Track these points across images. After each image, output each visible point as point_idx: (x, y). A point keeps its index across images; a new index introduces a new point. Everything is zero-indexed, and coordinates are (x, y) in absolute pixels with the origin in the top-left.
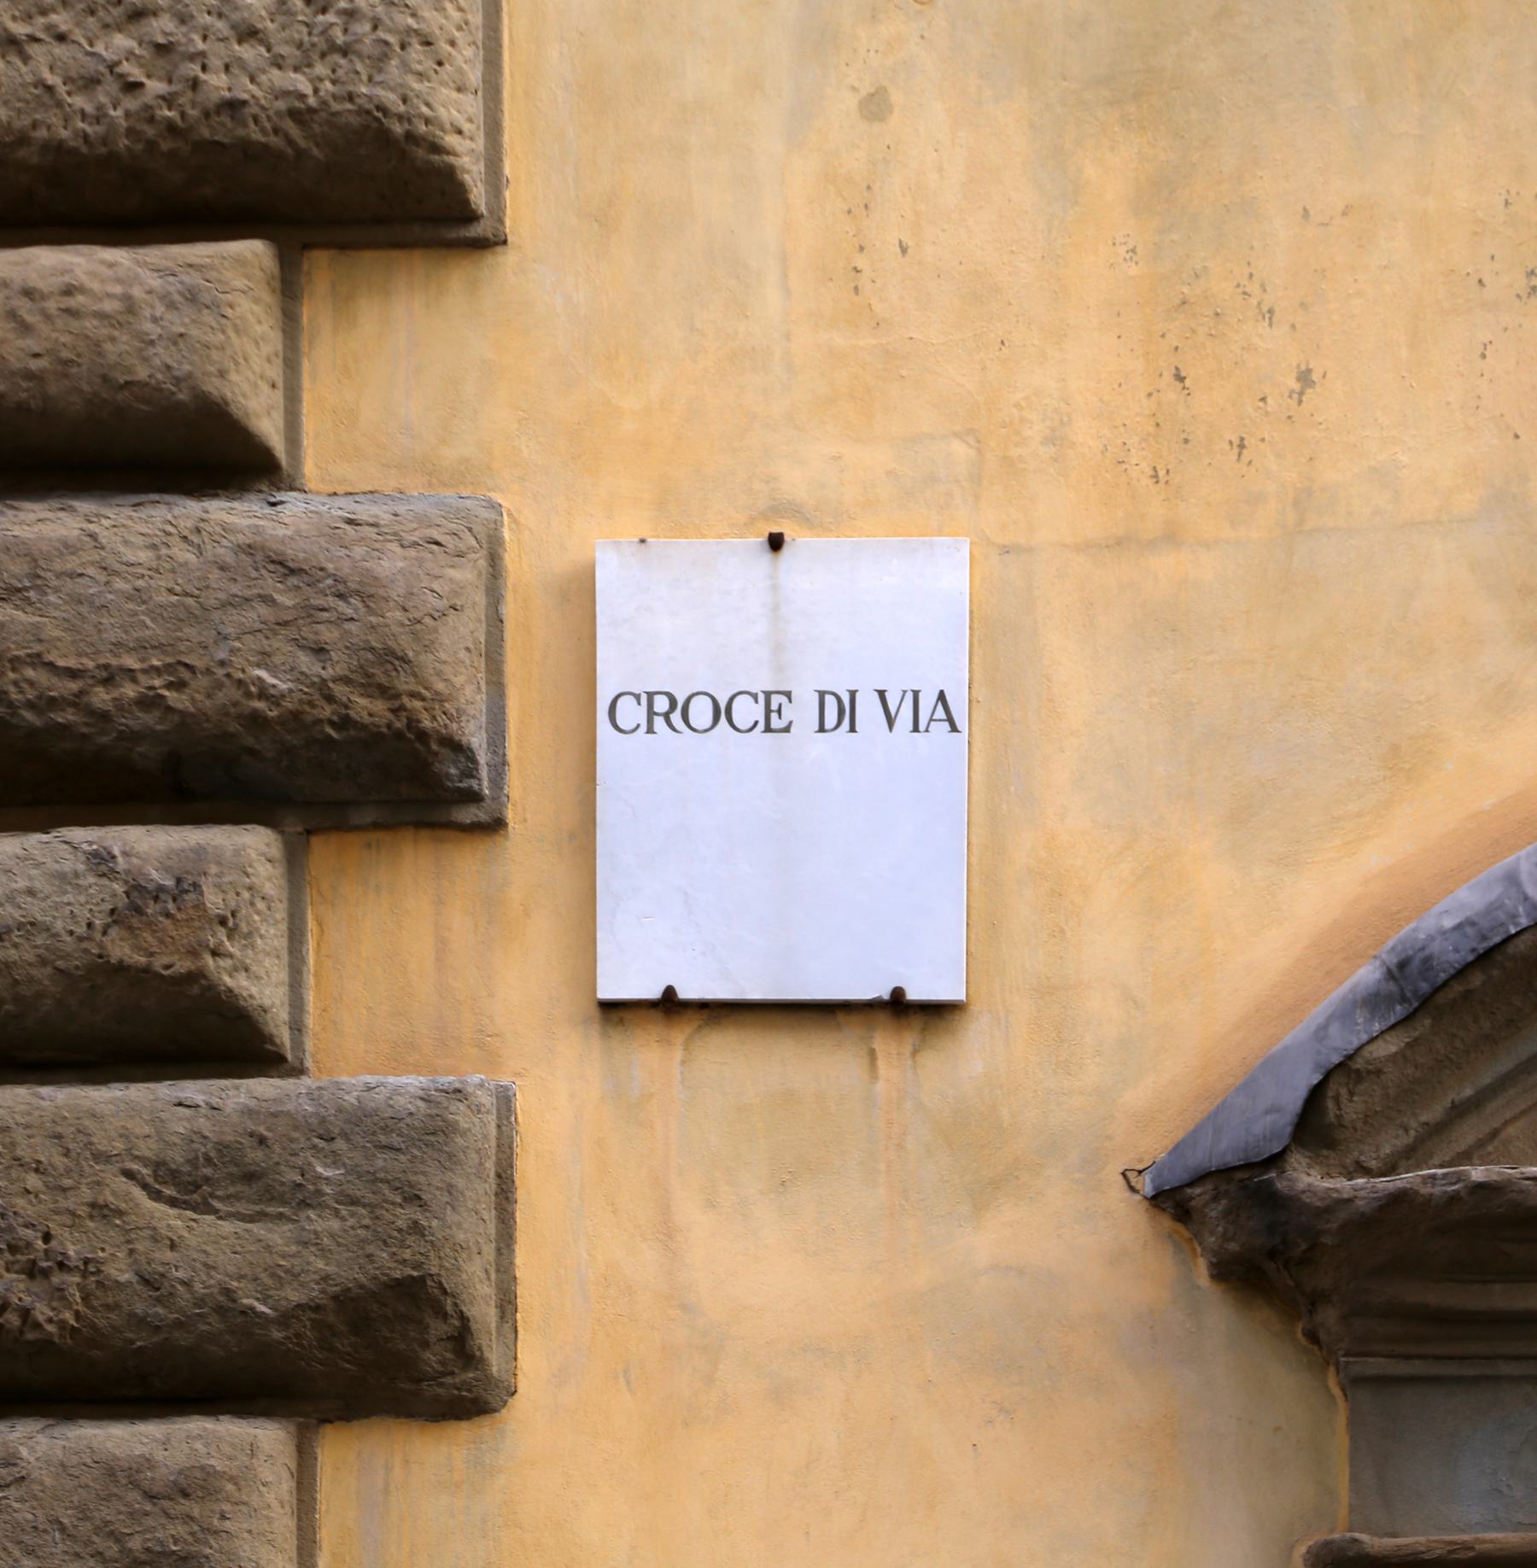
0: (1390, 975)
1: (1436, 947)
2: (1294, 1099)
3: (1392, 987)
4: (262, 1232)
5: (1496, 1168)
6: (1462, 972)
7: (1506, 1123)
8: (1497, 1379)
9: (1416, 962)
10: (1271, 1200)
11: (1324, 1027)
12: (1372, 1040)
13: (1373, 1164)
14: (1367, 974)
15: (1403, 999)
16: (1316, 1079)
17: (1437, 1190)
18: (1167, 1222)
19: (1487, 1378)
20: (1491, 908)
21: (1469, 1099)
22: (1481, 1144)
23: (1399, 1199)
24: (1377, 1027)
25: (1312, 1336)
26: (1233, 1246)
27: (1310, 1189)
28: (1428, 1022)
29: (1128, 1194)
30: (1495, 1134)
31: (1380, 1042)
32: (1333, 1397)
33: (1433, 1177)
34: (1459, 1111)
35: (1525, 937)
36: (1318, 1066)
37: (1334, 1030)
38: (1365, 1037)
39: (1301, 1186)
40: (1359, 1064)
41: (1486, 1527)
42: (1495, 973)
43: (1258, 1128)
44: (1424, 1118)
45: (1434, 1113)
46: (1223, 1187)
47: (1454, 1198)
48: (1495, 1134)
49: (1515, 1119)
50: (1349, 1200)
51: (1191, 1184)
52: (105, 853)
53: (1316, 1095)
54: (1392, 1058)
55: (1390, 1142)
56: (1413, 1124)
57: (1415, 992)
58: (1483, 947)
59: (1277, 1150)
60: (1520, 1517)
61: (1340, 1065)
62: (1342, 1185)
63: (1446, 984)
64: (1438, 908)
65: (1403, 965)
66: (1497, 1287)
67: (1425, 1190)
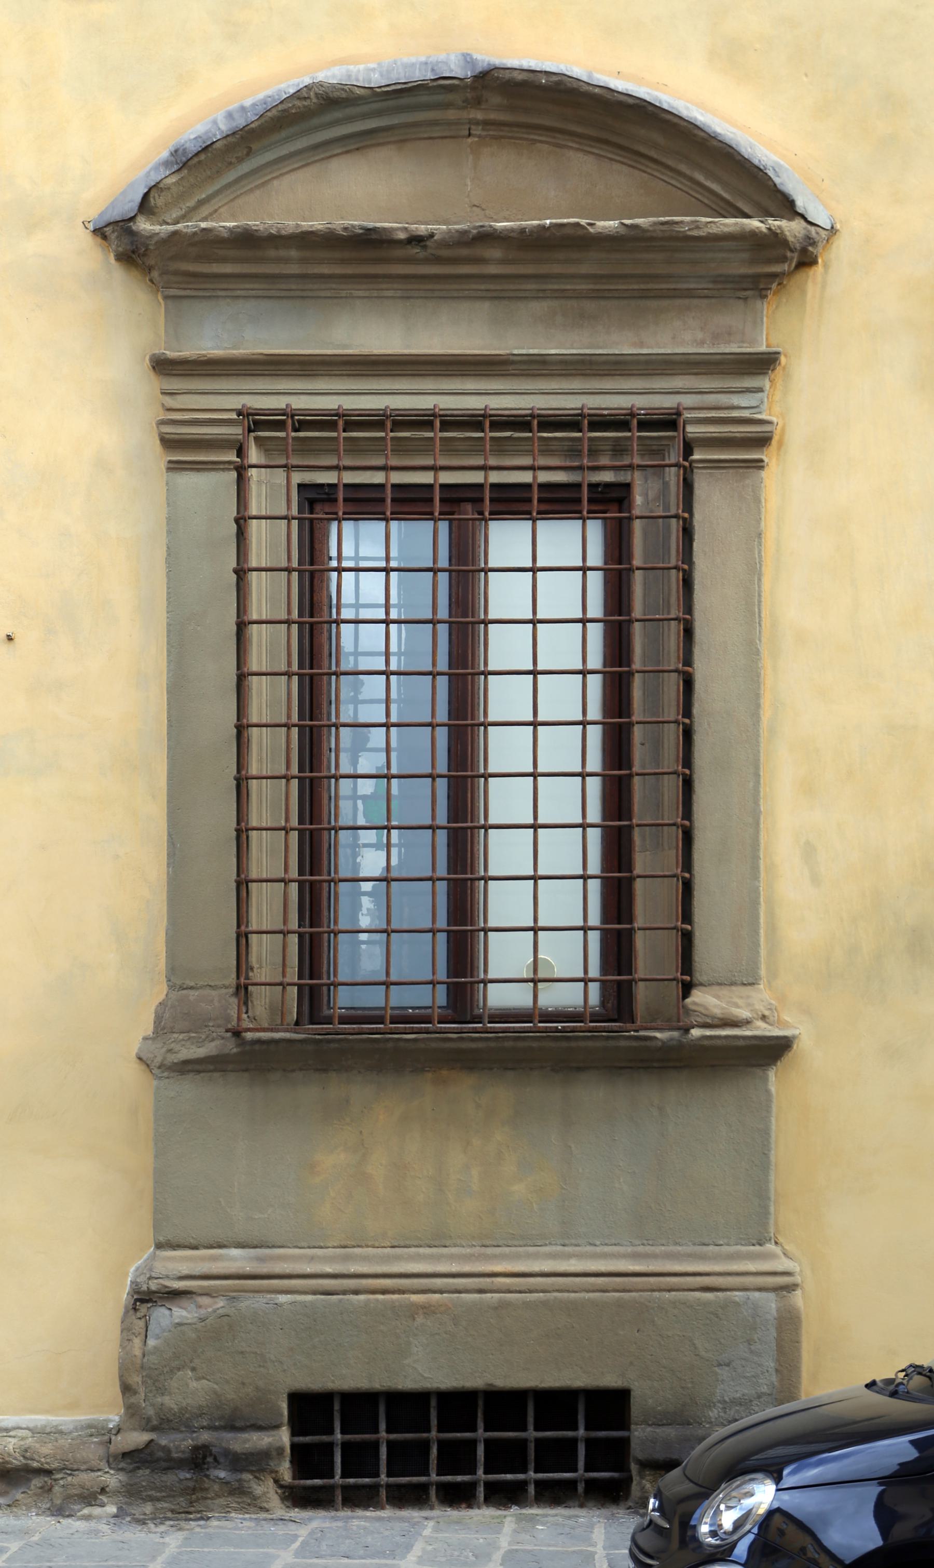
0: (172, 154)
1: (187, 145)
2: (138, 198)
3: (173, 158)
4: (468, 1250)
5: (210, 223)
6: (197, 154)
7: (220, 207)
8: (218, 297)
9: (181, 150)
10: (131, 233)
11: (149, 172)
12: (166, 177)
13: (169, 221)
14: (165, 154)
15: (177, 163)
16: (146, 190)
17: (189, 231)
18: (99, 240)
19: (214, 297)
20: (206, 133)
21: (204, 199)
22: (211, 214)
23: (175, 233)
24: (168, 173)
25: (151, 281)
26: (120, 249)
27: (144, 230)
28: (186, 171)
29: (85, 229)
30: (216, 211)
31: (169, 178)
32: (160, 303)
33: (188, 226)
34: (201, 203)
35: (219, 142)
36: (145, 187)
37: (152, 173)
38: (163, 176)
39: (141, 228)
40: (161, 185)
41: (213, 349)
42: (209, 155)
43: (127, 207)
44: (188, 205)
45: (191, 203)
46: (116, 228)
47: (195, 234)
48: (216, 211)
49: (223, 206)
50: (158, 234)
51: (105, 226)
52: (200, 1030)
53: (146, 196)
54: (174, 184)
55: (175, 214)
56: (184, 207)
57: (181, 160)
58: (204, 146)
59: (133, 215)
60: (226, 345)
61: (154, 186)
62: (157, 228)
63: (191, 158)
64: (190, 131)
65: (176, 151)
66: (214, 264)
67: (185, 230)
